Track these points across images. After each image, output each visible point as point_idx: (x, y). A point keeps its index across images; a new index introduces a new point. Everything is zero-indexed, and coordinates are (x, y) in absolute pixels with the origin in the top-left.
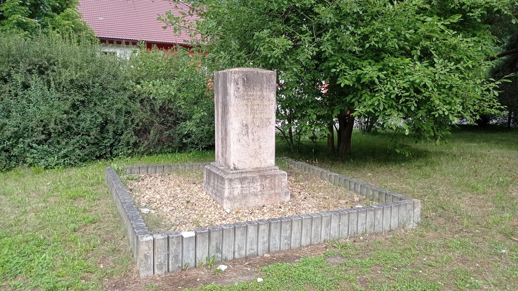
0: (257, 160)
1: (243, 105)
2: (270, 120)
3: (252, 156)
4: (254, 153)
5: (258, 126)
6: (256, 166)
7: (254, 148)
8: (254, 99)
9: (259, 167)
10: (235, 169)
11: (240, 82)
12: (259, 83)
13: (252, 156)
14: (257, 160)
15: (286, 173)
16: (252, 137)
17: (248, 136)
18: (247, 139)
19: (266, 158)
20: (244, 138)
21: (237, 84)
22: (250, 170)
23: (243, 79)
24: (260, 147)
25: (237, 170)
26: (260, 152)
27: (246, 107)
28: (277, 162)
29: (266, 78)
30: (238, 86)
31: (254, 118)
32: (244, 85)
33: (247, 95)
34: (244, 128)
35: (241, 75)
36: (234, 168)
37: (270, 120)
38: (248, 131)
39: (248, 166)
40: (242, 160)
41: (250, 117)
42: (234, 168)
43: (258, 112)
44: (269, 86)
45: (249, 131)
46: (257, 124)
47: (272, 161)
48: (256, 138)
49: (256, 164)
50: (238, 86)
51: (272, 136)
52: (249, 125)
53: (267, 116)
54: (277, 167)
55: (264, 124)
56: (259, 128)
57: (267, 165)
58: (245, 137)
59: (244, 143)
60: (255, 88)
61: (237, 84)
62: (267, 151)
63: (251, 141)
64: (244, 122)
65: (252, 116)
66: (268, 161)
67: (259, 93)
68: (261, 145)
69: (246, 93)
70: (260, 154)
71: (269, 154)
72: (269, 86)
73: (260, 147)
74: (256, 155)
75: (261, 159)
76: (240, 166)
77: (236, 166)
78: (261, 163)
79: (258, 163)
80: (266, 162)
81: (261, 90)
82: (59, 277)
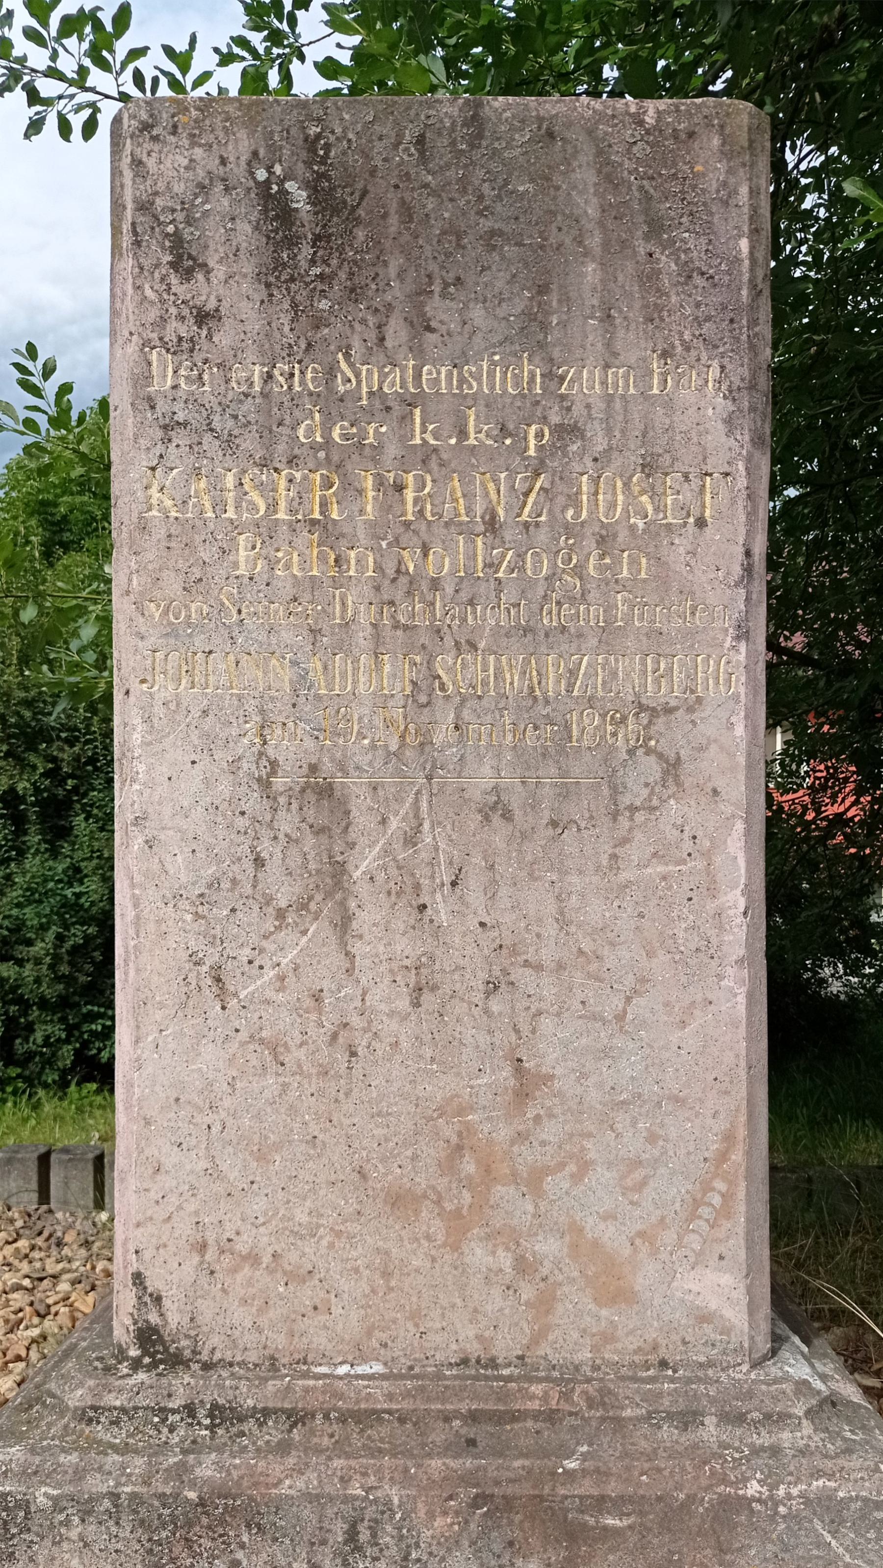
0: (478, 1255)
1: (266, 530)
2: (673, 736)
3: (400, 1201)
4: (431, 1153)
5: (496, 808)
6: (454, 1335)
7: (437, 1089)
8: (427, 456)
9: (505, 1346)
10: (156, 1348)
11: (231, 236)
12: (491, 240)
13: (400, 1201)
14: (478, 1255)
15: (262, 513)
16: (405, 947)
17: (343, 924)
18: (326, 970)
19: (613, 1237)
20: (290, 948)
21: (185, 262)
22: (362, 1375)
23: (274, 206)
24: (526, 1083)
25: (176, 1361)
26: (528, 1156)
27: (300, 559)
28: (796, 1305)
29: (609, 177)
30: (204, 291)
31: (424, 693)
32: (276, 275)
33: (332, 404)
34: (287, 822)
35: (241, 145)
36: (147, 1336)
37: (673, 736)
38: (338, 872)
39: (348, 1320)
40: (266, 1242)
41: (370, 684)
42: (147, 1336)
43: (488, 619)
44: (649, 278)
45: (364, 863)
46: (482, 779)
47: (717, 1284)
48: (464, 957)
49: (468, 1313)
50: (204, 291)
51: (708, 950)
52: (356, 787)
53: (633, 674)
54: (805, 1368)
55: (580, 781)
56: (499, 835)
57: (635, 1333)
58: (303, 946)
59: (282, 1022)
60: (437, 308)
61: (185, 262)
62: (633, 1144)
63: (387, 996)
64: (290, 748)
65: (395, 675)
66: (645, 1277)
67: (498, 377)
68: (548, 1054)
69: (310, 378)
70: (534, 1182)
71: (670, 1189)
72: (649, 278)
73: (526, 1083)
74: (462, 1179)
75: (548, 1247)
76: (225, 1317)
77: (174, 1318)
78: (545, 1303)
79: (495, 1301)
80: (614, 1290)
81: (532, 332)
82: (740, 1419)
